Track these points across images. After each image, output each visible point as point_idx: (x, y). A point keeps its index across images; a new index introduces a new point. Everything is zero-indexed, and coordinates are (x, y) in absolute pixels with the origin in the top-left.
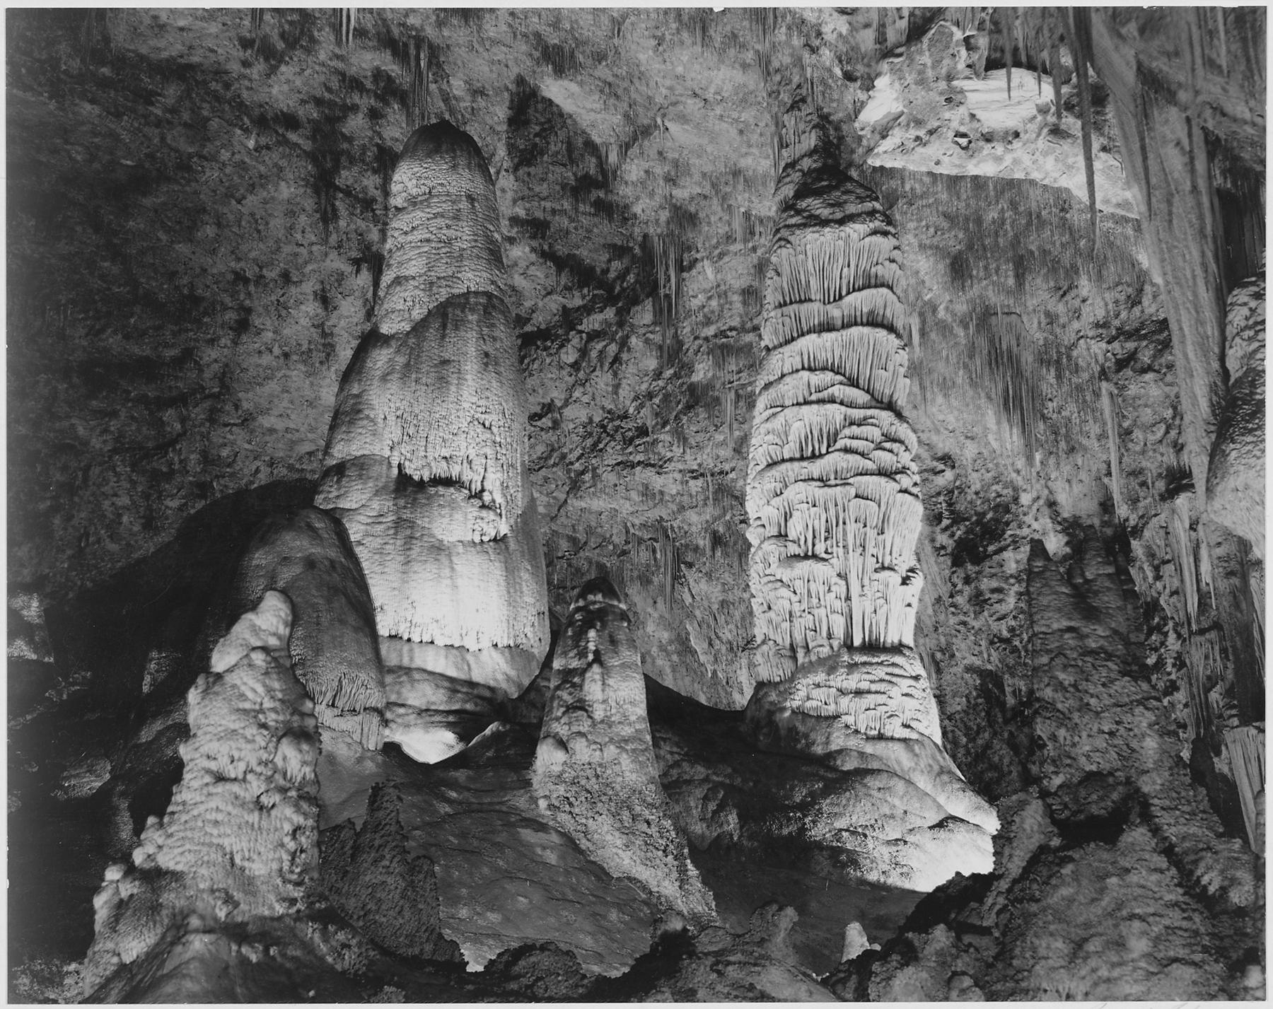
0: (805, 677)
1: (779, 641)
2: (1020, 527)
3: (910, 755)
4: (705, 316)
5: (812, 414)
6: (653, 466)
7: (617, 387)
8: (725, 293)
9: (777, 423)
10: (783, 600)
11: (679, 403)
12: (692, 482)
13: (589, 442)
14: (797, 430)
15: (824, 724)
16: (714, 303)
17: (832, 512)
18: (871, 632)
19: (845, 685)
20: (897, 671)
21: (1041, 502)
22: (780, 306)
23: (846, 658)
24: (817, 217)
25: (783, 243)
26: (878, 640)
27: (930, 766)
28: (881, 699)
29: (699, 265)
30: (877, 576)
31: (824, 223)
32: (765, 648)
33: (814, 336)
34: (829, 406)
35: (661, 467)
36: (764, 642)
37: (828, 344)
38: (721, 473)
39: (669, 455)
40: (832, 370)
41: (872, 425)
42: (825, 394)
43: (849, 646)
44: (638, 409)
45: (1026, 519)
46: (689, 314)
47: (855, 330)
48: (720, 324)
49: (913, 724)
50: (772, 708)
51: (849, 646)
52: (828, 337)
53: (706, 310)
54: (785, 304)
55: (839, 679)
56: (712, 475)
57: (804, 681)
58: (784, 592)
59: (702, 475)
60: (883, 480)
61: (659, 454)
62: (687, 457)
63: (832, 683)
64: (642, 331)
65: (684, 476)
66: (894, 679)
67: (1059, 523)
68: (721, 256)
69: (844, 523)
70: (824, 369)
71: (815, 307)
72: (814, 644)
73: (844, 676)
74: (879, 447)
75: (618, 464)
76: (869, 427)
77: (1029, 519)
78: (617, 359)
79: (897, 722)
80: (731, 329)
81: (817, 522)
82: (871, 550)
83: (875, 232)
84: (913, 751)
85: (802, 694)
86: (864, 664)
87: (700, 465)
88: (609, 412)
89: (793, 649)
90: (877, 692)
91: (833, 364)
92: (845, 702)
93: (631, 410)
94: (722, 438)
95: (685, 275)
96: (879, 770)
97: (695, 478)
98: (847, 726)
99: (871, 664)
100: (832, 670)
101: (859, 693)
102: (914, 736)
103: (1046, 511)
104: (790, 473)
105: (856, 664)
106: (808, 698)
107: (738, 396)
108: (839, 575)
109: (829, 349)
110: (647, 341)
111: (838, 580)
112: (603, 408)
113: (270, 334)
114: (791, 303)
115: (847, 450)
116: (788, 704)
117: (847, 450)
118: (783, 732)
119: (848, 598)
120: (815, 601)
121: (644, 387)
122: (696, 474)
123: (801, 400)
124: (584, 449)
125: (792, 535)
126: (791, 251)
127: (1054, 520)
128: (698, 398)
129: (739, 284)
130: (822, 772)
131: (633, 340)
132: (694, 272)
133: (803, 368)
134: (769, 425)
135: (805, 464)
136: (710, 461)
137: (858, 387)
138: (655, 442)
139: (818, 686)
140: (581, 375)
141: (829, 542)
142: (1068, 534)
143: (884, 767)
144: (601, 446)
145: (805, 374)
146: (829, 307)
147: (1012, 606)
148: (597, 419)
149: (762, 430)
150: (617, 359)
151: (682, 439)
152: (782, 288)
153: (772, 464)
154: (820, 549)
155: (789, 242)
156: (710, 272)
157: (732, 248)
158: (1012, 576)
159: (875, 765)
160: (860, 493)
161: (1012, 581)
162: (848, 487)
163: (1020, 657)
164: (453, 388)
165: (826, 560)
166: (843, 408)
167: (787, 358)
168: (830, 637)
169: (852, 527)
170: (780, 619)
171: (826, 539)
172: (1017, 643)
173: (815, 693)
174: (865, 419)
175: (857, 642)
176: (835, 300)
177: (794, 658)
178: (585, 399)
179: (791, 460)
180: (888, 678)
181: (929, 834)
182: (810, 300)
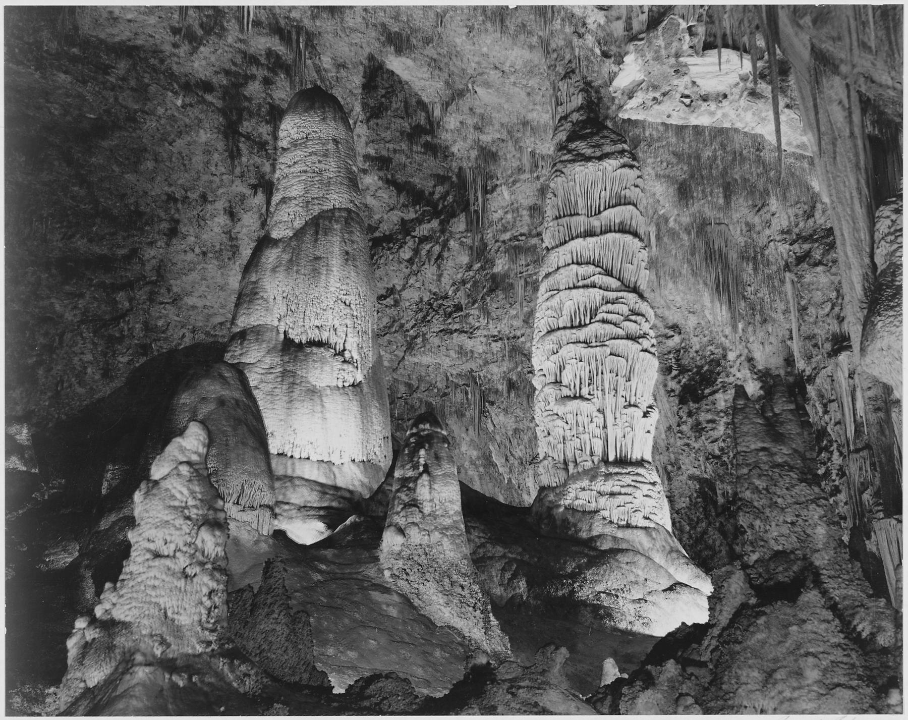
0: (574, 483)
1: (556, 457)
2: (727, 376)
3: (650, 539)
4: (503, 225)
5: (579, 296)
6: (466, 332)
7: (440, 276)
8: (517, 209)
9: (554, 302)
10: (559, 428)
11: (484, 287)
12: (493, 344)
13: (420, 315)
14: (569, 307)
15: (588, 517)
16: (509, 216)
17: (594, 365)
18: (621, 451)
19: (603, 489)
20: (640, 479)
21: (743, 358)
22: (557, 218)
23: (603, 469)
24: (583, 155)
25: (558, 173)
26: (626, 456)
27: (664, 546)
28: (628, 499)
29: (499, 189)
30: (625, 411)
31: (588, 159)
32: (546, 462)
33: (580, 240)
34: (591, 290)
35: (471, 333)
36: (545, 458)
37: (591, 246)
38: (514, 337)
39: (477, 324)
40: (594, 264)
41: (622, 303)
42: (588, 281)
43: (605, 461)
44: (455, 292)
45: (732, 370)
46: (491, 224)
47: (610, 236)
48: (514, 232)
49: (651, 517)
50: (551, 505)
51: (605, 461)
52: (591, 240)
53: (503, 221)
54: (560, 217)
55: (599, 484)
56: (508, 339)
57: (574, 486)
58: (559, 422)
59: (501, 339)
60: (630, 342)
61: (470, 324)
62: (490, 326)
63: (593, 488)
64: (458, 236)
65: (488, 339)
66: (638, 485)
67: (756, 373)
68: (514, 183)
69: (602, 373)
70: (588, 263)
71: (582, 219)
72: (581, 459)
73: (602, 483)
74: (627, 319)
75: (441, 331)
76: (620, 305)
77: (734, 370)
78: (440, 256)
79: (640, 515)
80: (521, 235)
81: (582, 372)
82: (621, 392)
83: (624, 166)
84: (651, 536)
85: (572, 495)
86: (617, 474)
87: (499, 332)
88: (434, 294)
89: (565, 463)
90: (625, 494)
91: (594, 260)
92: (602, 501)
93: (450, 293)
94: (515, 312)
95: (489, 196)
96: (627, 550)
97: (496, 341)
98: (604, 518)
99: (621, 474)
100: (593, 478)
101: (612, 494)
102: (652, 525)
103: (746, 364)
104: (564, 338)
105: (611, 474)
106: (577, 498)
107: (526, 283)
108: (598, 410)
109: (591, 249)
110: (462, 244)
111: (597, 414)
112: (430, 291)
113: (193, 239)
114: (564, 216)
115: (604, 321)
116: (562, 502)
117: (604, 321)
118: (558, 523)
119: (605, 427)
120: (581, 429)
121: (459, 276)
122: (496, 339)
123: (571, 286)
124: (416, 320)
125: (565, 381)
126: (564, 179)
127: (751, 371)
128: (497, 284)
129: (527, 202)
130: (586, 551)
131: (452, 243)
132: (495, 194)
133: (573, 263)
134: (548, 304)
135: (574, 331)
136: (506, 329)
137: (612, 276)
138: (467, 315)
139: (583, 489)
140: (415, 267)
141: (591, 387)
142: (762, 381)
143: (630, 548)
144: (429, 318)
145: (575, 267)
146: (591, 219)
147: (722, 433)
148: (426, 299)
149: (544, 307)
150: (440, 256)
151: (487, 314)
152: (558, 206)
153: (551, 331)
154: (585, 392)
155: (563, 173)
156: (506, 194)
157: (523, 177)
158: (721, 411)
159: (624, 546)
160: (613, 352)
161: (722, 414)
162: (605, 348)
163: (727, 469)
164: (323, 277)
165: (589, 400)
166: (601, 291)
167: (562, 255)
168: (592, 454)
169: (607, 376)
170: (556, 441)
171: (589, 385)
172: (725, 459)
173: (582, 495)
174: (617, 299)
175: (611, 458)
176: (595, 214)
177: (567, 470)
178: (418, 285)
179: (565, 328)
180: (633, 484)
181: (663, 595)
182: (578, 214)
